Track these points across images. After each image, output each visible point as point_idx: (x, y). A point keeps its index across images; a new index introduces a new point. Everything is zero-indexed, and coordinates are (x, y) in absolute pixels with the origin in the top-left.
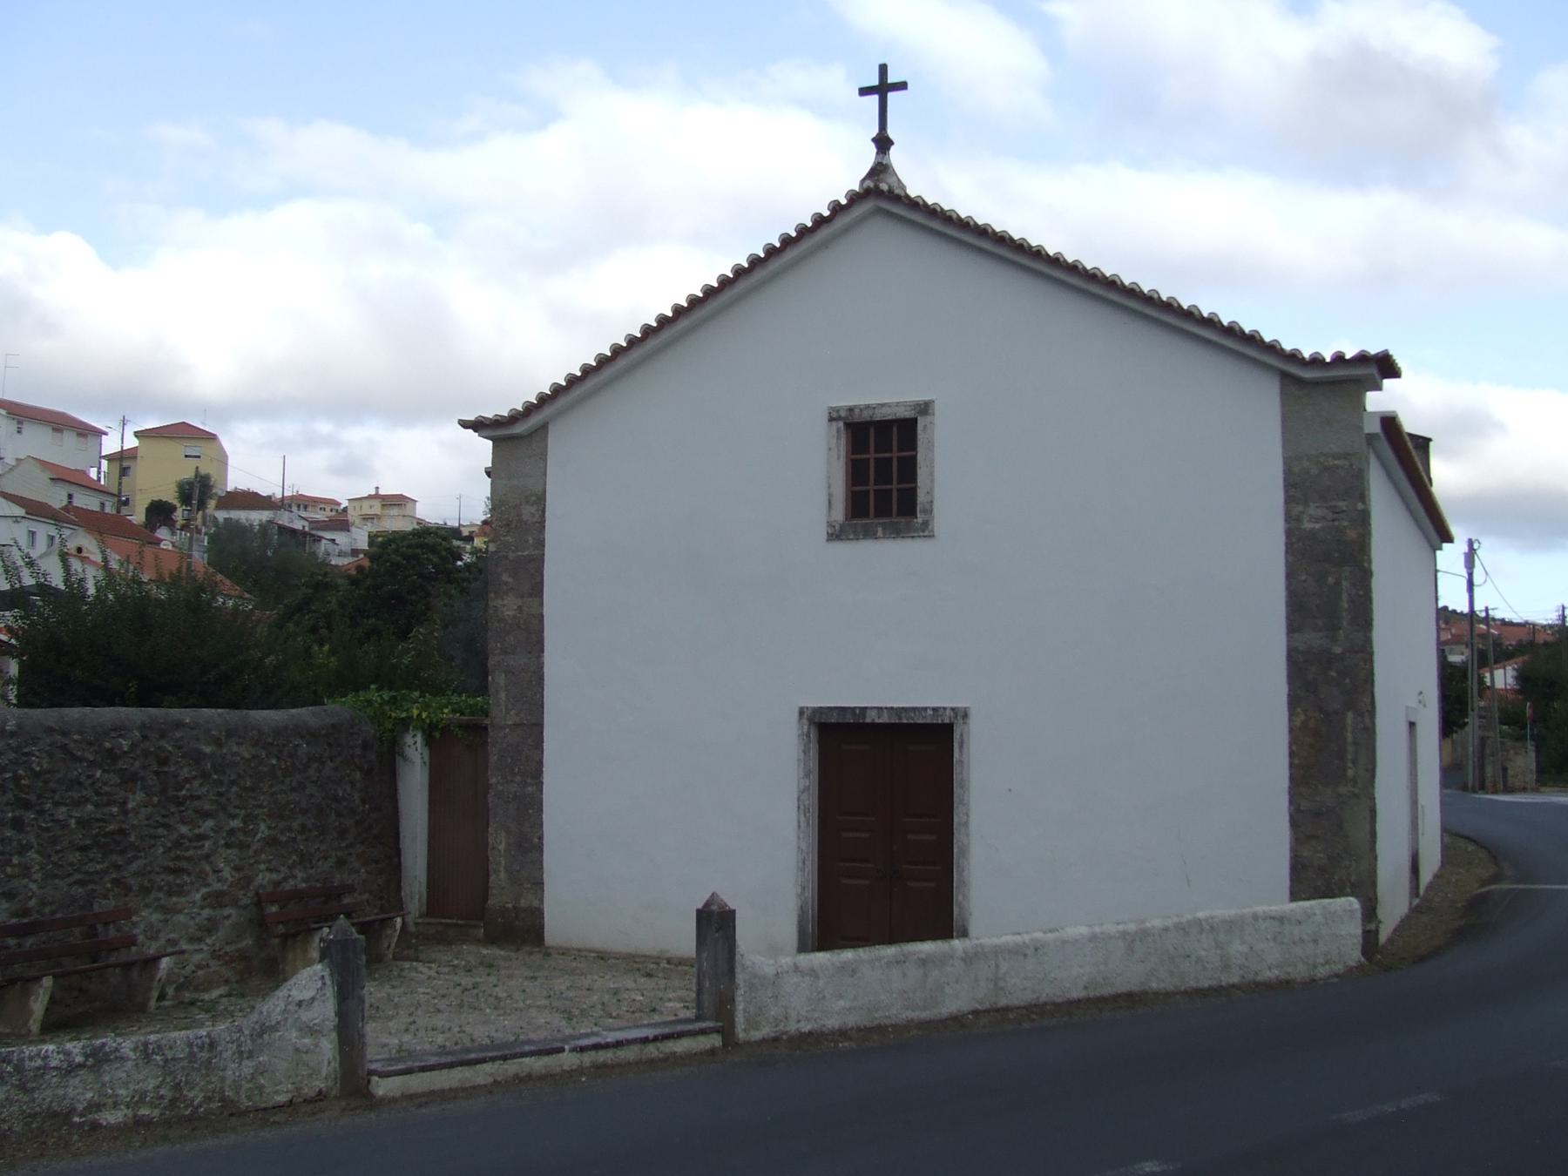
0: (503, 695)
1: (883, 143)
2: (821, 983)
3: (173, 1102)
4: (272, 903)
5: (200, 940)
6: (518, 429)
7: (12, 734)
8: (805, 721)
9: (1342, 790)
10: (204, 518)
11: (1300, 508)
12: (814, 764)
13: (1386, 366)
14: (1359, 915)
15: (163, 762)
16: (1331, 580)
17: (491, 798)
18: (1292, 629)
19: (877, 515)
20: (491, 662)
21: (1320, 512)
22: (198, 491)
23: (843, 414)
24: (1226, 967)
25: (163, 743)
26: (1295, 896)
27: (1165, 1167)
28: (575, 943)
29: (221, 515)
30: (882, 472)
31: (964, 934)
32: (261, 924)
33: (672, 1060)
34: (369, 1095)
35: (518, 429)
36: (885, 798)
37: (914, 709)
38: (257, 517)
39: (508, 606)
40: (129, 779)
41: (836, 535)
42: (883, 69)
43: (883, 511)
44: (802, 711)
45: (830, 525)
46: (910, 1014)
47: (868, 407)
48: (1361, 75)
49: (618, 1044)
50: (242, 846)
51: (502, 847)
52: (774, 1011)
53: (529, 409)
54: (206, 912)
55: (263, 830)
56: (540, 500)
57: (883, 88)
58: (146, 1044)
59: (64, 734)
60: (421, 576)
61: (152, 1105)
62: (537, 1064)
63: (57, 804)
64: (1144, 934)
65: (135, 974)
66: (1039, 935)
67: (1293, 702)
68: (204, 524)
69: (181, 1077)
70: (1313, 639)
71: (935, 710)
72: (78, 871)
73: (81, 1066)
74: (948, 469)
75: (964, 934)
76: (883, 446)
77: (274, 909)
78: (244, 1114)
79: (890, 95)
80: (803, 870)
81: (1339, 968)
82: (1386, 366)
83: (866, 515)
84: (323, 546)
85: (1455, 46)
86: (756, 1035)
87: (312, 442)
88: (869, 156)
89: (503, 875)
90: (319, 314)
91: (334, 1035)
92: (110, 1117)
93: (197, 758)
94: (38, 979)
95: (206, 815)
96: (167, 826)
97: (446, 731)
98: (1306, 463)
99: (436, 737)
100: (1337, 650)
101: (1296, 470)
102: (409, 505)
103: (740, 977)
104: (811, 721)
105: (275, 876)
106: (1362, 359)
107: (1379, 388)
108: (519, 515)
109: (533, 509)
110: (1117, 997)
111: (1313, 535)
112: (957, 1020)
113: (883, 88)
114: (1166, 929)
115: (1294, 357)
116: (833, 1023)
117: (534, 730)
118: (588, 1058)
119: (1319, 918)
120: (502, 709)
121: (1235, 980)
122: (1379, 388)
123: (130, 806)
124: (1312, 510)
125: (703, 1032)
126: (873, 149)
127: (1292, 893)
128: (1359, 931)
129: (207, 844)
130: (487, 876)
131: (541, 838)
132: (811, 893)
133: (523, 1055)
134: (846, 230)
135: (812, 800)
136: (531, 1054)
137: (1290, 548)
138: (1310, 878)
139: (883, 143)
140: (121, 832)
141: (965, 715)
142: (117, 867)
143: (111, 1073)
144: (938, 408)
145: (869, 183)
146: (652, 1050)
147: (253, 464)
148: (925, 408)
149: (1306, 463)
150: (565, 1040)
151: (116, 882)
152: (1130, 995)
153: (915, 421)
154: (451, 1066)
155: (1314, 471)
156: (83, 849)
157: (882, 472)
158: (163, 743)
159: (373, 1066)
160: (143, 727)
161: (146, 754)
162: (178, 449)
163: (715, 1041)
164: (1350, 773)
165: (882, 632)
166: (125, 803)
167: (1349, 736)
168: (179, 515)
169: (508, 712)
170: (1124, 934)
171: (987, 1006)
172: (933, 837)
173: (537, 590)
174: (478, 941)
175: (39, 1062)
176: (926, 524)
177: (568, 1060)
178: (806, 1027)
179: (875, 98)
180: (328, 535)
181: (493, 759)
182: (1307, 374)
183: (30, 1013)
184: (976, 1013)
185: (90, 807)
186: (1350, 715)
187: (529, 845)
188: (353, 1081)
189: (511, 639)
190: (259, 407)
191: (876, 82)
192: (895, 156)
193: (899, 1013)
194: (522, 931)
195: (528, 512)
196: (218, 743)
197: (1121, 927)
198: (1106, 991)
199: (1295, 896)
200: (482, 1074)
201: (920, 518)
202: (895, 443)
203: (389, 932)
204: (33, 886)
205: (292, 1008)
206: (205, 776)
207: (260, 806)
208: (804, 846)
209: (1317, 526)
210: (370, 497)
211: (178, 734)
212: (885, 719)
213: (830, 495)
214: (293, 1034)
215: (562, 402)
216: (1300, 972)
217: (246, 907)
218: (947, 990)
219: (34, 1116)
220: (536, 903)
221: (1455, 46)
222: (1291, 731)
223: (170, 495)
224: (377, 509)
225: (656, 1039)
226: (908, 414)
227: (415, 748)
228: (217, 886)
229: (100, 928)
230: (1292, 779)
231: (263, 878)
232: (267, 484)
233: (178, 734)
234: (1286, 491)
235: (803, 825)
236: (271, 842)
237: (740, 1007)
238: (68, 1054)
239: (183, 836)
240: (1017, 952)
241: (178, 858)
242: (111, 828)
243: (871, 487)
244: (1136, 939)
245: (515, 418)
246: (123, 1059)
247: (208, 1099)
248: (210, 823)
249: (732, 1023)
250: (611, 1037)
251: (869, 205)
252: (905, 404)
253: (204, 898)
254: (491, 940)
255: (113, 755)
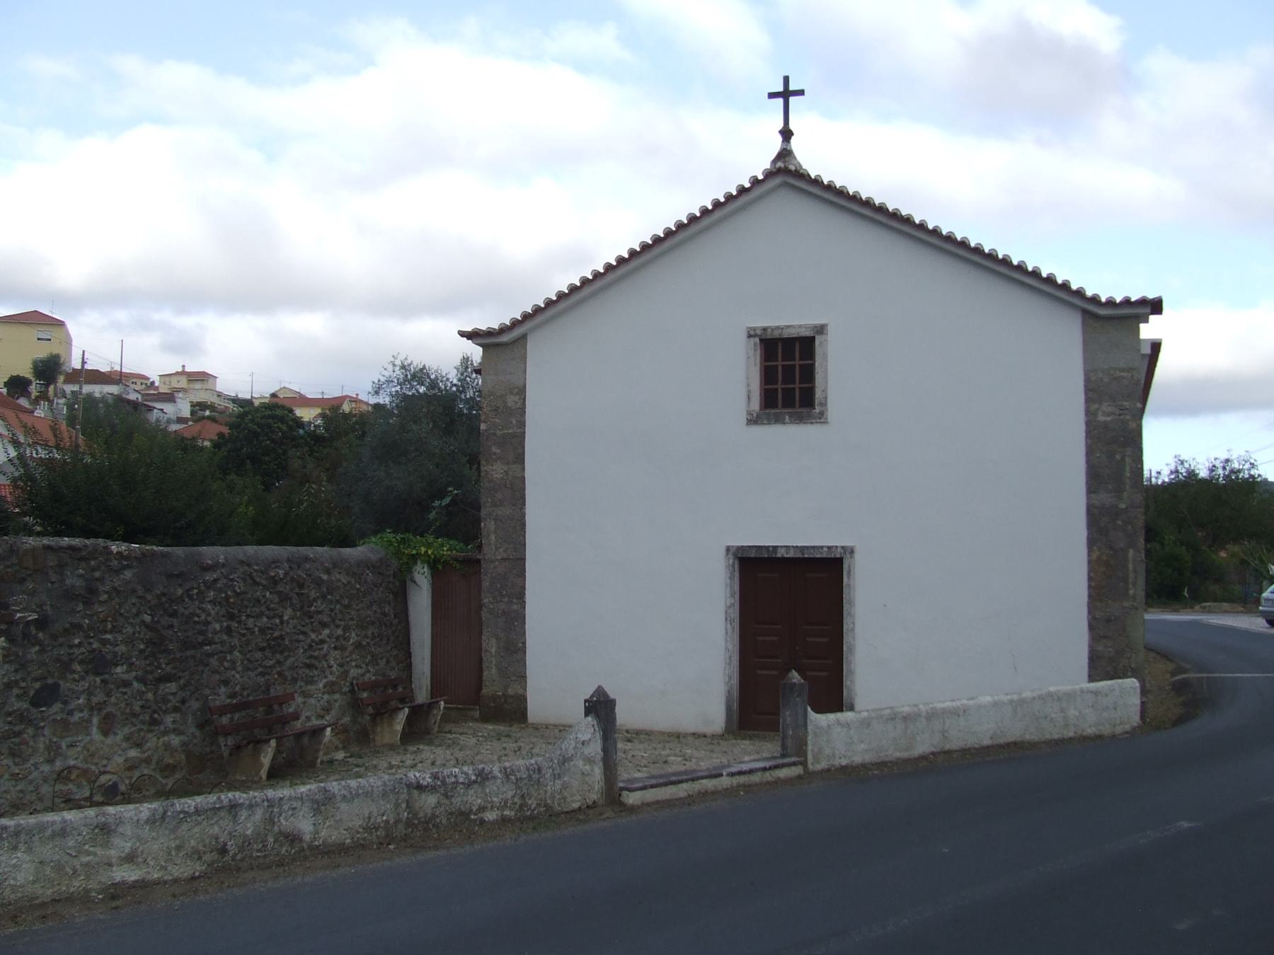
0: (493, 537)
1: (786, 134)
2: (852, 732)
3: (521, 806)
4: (364, 690)
5: (323, 717)
6: (505, 338)
7: (223, 565)
8: (731, 556)
9: (1126, 604)
10: (55, 388)
11: (1096, 406)
12: (737, 588)
13: (1155, 306)
14: (1138, 691)
15: (301, 586)
16: (1118, 457)
17: (484, 614)
18: (1090, 491)
19: (784, 406)
20: (483, 512)
21: (1110, 409)
22: (49, 369)
23: (759, 332)
24: (1067, 725)
25: (300, 572)
26: (1092, 678)
27: (1193, 825)
28: (552, 720)
29: (69, 388)
30: (788, 375)
31: (851, 708)
32: (355, 705)
33: (777, 782)
34: (622, 804)
35: (505, 338)
36: (791, 613)
37: (814, 547)
38: (97, 390)
39: (495, 471)
40: (284, 598)
41: (753, 420)
42: (786, 79)
43: (789, 402)
44: (728, 549)
45: (749, 413)
46: (898, 754)
47: (778, 328)
48: (1026, 48)
49: (751, 771)
50: (343, 649)
51: (493, 650)
52: (827, 751)
53: (515, 324)
54: (326, 697)
55: (353, 638)
56: (522, 392)
57: (786, 94)
58: (505, 769)
59: (249, 565)
60: (273, 441)
61: (511, 809)
62: (709, 784)
63: (248, 616)
64: (1022, 702)
65: (306, 740)
66: (965, 702)
67: (1091, 543)
68: (56, 395)
69: (525, 790)
70: (1106, 498)
71: (829, 548)
72: (260, 665)
73: (475, 782)
74: (837, 373)
75: (851, 708)
76: (788, 355)
77: (365, 695)
78: (558, 815)
79: (791, 99)
80: (729, 664)
81: (1128, 727)
82: (1155, 306)
83: (776, 406)
84: (154, 416)
85: (1102, 32)
86: (819, 767)
87: (145, 326)
88: (776, 143)
89: (494, 671)
90: (246, 237)
91: (601, 764)
92: (490, 816)
93: (318, 583)
94: (269, 740)
95: (324, 625)
96: (304, 633)
97: (446, 563)
98: (1100, 375)
99: (438, 568)
100: (1123, 506)
101: (1093, 379)
102: (211, 380)
103: (810, 728)
104: (735, 555)
105: (359, 671)
106: (1143, 302)
107: (1147, 321)
108: (505, 402)
109: (516, 398)
110: (1008, 745)
111: (1106, 426)
112: (923, 758)
113: (786, 94)
114: (1034, 698)
115: (1095, 300)
116: (858, 759)
117: (518, 563)
118: (742, 779)
119: (1117, 693)
120: (492, 546)
121: (1071, 734)
122: (1147, 321)
123: (286, 618)
124: (1106, 407)
125: (794, 764)
126: (780, 139)
127: (1089, 676)
128: (1138, 702)
129: (326, 646)
130: (481, 670)
131: (524, 643)
132: (735, 681)
133: (702, 778)
134: (761, 197)
135: (735, 613)
136: (706, 777)
137: (1089, 434)
138: (1101, 667)
139: (786, 134)
140: (282, 638)
141: (852, 552)
142: (279, 662)
143: (491, 787)
144: (831, 330)
145: (780, 164)
146: (768, 776)
147: (95, 343)
148: (821, 329)
149: (1100, 375)
150: (724, 767)
151: (280, 674)
152: (1015, 743)
153: (813, 338)
154: (666, 784)
155: (1106, 380)
156: (262, 649)
157: (788, 375)
158: (300, 572)
159: (621, 785)
160: (289, 560)
161: (293, 579)
162: (31, 333)
163: (798, 770)
164: (1131, 592)
165: (789, 494)
166: (281, 617)
167: (1130, 566)
168: (34, 389)
169: (497, 549)
170: (1011, 702)
171: (938, 750)
172: (825, 640)
173: (520, 459)
174: (475, 720)
175: (453, 780)
176: (822, 414)
177: (725, 782)
178: (844, 762)
179: (780, 101)
180: (158, 405)
181: (486, 584)
182: (1091, 308)
183: (262, 765)
184: (933, 753)
185: (265, 619)
186: (1131, 551)
187: (515, 649)
188: (613, 795)
189: (499, 495)
190: (108, 296)
191: (781, 89)
192: (795, 143)
193: (894, 754)
194: (510, 711)
195: (511, 400)
196: (328, 572)
197: (1009, 697)
198: (1002, 741)
199: (1092, 678)
200: (681, 791)
201: (817, 409)
202: (797, 354)
203: (435, 712)
204: (237, 676)
205: (580, 745)
206: (324, 597)
207: (352, 619)
208: (730, 647)
209: (1109, 419)
210: (177, 373)
211: (307, 566)
212: (791, 554)
213: (749, 392)
214: (581, 763)
215: (539, 319)
216: (1106, 730)
217: (345, 694)
218: (918, 738)
219: (451, 814)
220: (520, 691)
221: (1102, 32)
222: (1089, 562)
223: (26, 371)
224: (183, 383)
225: (770, 768)
226: (808, 333)
227: (422, 578)
228: (331, 678)
229: (276, 707)
230: (1090, 596)
231: (354, 672)
232: (98, 363)
233: (307, 566)
234: (1086, 394)
235: (730, 631)
236: (358, 646)
237: (810, 748)
238: (466, 774)
239: (313, 641)
240: (955, 713)
241: (311, 657)
242: (276, 634)
243: (780, 386)
244: (1019, 704)
245: (503, 330)
246: (495, 778)
247: (539, 805)
248: (327, 632)
249: (806, 761)
250: (745, 767)
251: (778, 180)
252: (805, 326)
253: (325, 687)
254: (485, 719)
255: (275, 581)
